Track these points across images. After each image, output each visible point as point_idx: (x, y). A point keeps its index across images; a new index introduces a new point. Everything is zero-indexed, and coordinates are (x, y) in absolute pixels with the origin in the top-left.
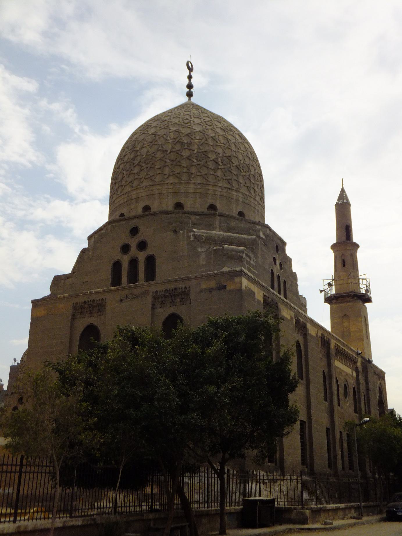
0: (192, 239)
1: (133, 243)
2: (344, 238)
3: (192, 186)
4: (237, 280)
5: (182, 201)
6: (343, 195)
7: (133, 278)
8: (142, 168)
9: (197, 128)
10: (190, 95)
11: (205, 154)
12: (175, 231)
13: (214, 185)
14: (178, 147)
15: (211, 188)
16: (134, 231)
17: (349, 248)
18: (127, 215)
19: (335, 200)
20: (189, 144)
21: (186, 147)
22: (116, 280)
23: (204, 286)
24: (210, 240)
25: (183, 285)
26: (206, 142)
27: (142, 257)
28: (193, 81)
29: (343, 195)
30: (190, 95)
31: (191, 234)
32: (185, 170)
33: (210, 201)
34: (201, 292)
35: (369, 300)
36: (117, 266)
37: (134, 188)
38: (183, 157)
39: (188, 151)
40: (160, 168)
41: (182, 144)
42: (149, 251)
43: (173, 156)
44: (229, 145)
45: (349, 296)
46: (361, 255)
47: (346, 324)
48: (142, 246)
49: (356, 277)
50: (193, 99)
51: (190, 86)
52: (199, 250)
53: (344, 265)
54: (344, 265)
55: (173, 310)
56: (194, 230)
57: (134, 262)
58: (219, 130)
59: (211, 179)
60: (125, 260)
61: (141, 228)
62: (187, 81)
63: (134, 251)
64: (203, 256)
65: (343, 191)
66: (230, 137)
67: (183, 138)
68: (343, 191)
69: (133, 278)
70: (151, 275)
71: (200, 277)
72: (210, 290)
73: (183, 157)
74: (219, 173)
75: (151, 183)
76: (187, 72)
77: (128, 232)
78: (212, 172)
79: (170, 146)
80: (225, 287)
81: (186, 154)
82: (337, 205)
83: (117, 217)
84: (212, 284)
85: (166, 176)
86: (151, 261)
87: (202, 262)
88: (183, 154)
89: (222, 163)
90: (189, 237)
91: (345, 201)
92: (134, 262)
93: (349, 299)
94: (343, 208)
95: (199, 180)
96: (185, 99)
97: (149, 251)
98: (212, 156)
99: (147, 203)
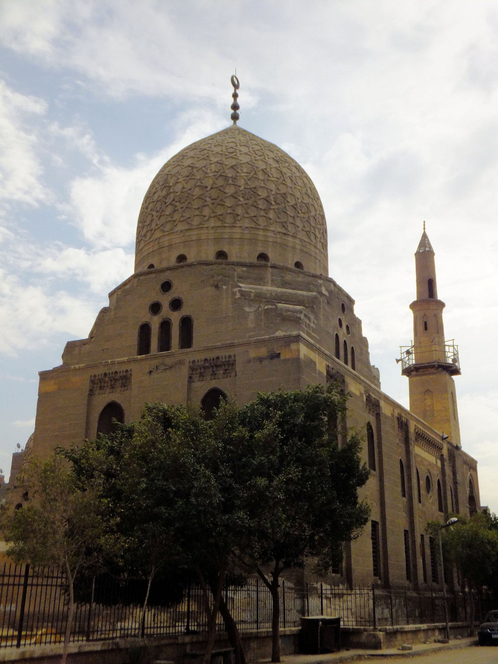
0: (238, 295)
1: (165, 301)
2: (426, 295)
3: (238, 230)
4: (293, 346)
5: (226, 250)
6: (424, 241)
7: (165, 344)
8: (176, 208)
9: (244, 159)
10: (235, 117)
11: (254, 191)
12: (217, 286)
13: (265, 230)
14: (220, 182)
15: (261, 233)
16: (166, 286)
17: (431, 307)
18: (157, 266)
19: (415, 248)
20: (234, 178)
21: (230, 182)
22: (144, 347)
23: (253, 354)
24: (259, 297)
25: (227, 354)
27: (175, 318)
28: (239, 100)
29: (424, 241)
30: (235, 117)
31: (236, 289)
32: (229, 211)
33: (260, 249)
34: (249, 361)
35: (456, 371)
36: (145, 330)
38: (227, 195)
39: (233, 187)
40: (199, 208)
41: (226, 178)
42: (185, 311)
44: (284, 180)
45: (433, 367)
46: (447, 316)
47: (428, 402)
48: (176, 304)
49: (441, 343)
50: (238, 122)
52: (247, 309)
53: (426, 329)
54: (426, 329)
55: (214, 384)
56: (241, 285)
57: (166, 325)
58: (271, 161)
59: (262, 222)
60: (155, 323)
61: (175, 283)
62: (231, 101)
63: (166, 310)
64: (252, 317)
65: (425, 236)
66: (284, 170)
67: (227, 171)
68: (425, 236)
70: (186, 341)
71: (248, 344)
72: (260, 360)
73: (227, 195)
74: (271, 215)
76: (232, 90)
77: (159, 287)
78: (262, 213)
79: (211, 181)
80: (278, 355)
81: (230, 190)
82: (417, 254)
84: (263, 352)
85: (206, 219)
86: (187, 323)
87: (251, 325)
88: (227, 191)
89: (275, 202)
90: (234, 294)
91: (427, 249)
92: (166, 325)
93: (432, 370)
94: (425, 257)
95: (247, 223)
97: (185, 311)
98: (263, 194)
99: (182, 252)
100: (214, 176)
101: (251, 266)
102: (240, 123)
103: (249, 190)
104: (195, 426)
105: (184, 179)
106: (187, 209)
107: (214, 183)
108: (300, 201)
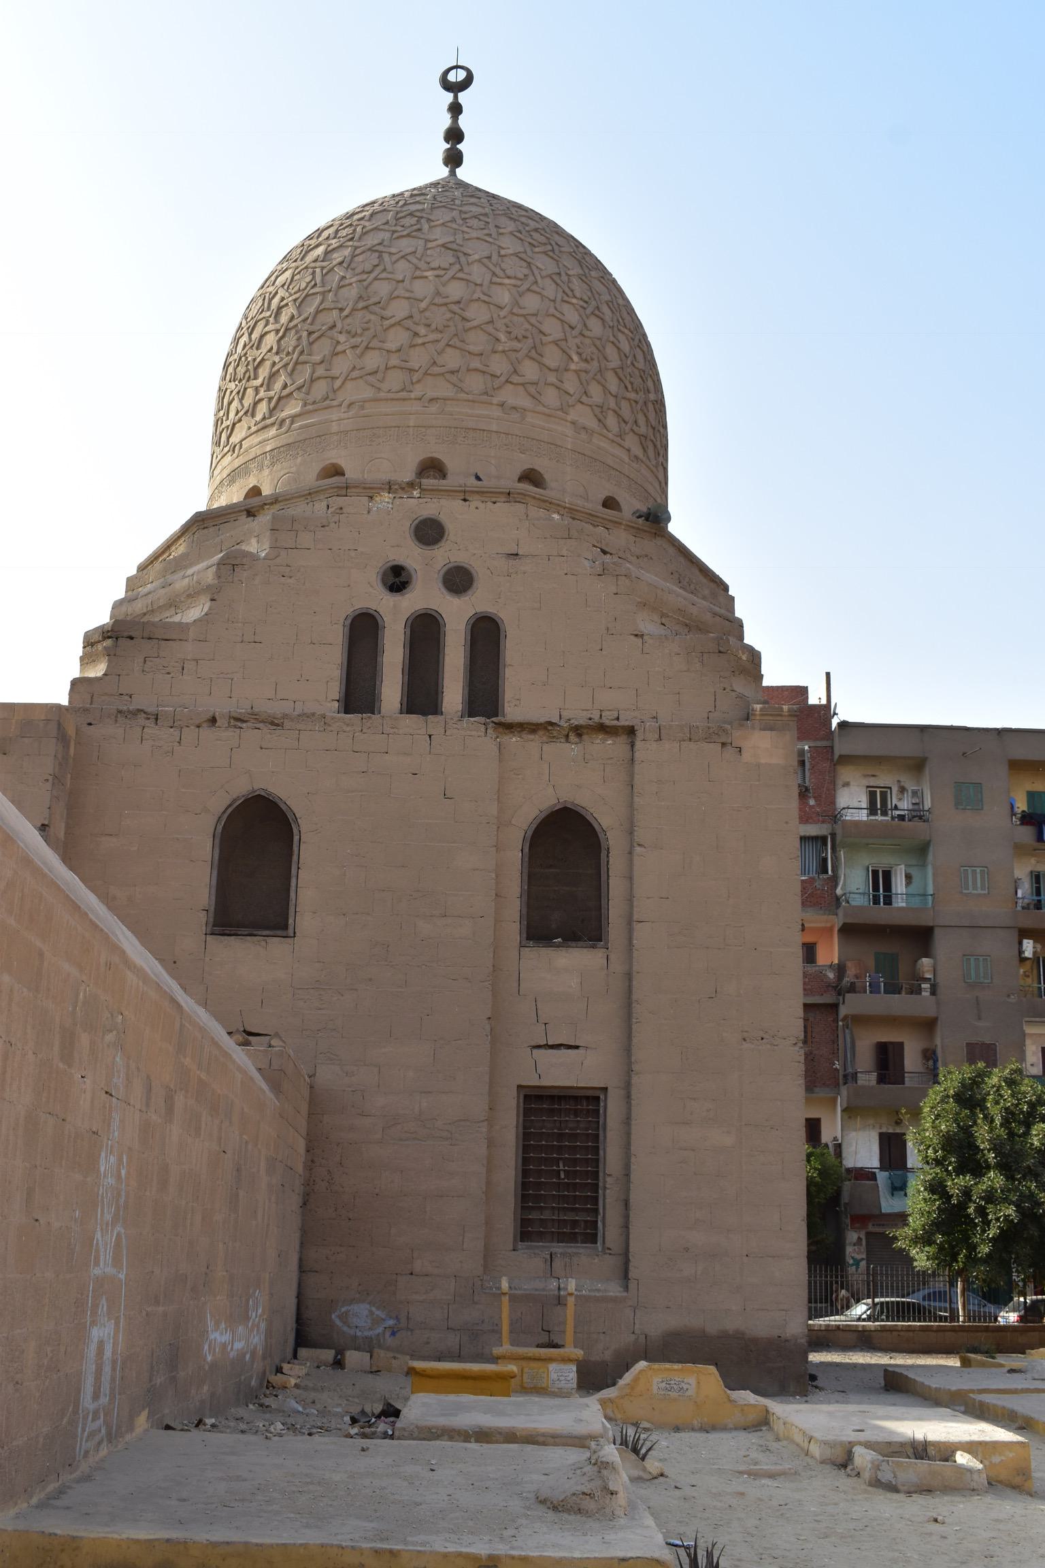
7: (422, 698)
8: (339, 348)
10: (454, 159)
18: (351, 474)
22: (358, 696)
26: (460, 275)
27: (456, 615)
30: (454, 159)
36: (364, 629)
37: (382, 395)
38: (468, 325)
39: (405, 303)
40: (322, 362)
43: (439, 316)
50: (461, 173)
51: (454, 135)
57: (425, 630)
60: (394, 614)
62: (446, 121)
69: (422, 698)
73: (468, 325)
75: (369, 393)
76: (463, 122)
80: (391, 1412)
83: (310, 478)
86: (486, 635)
89: (579, 354)
92: (425, 630)
96: (444, 172)
100: (437, 276)
101: (591, 518)
102: (462, 173)
103: (522, 319)
104: (261, 1405)
105: (359, 278)
106: (449, 350)
107: (438, 293)
108: (277, 359)
